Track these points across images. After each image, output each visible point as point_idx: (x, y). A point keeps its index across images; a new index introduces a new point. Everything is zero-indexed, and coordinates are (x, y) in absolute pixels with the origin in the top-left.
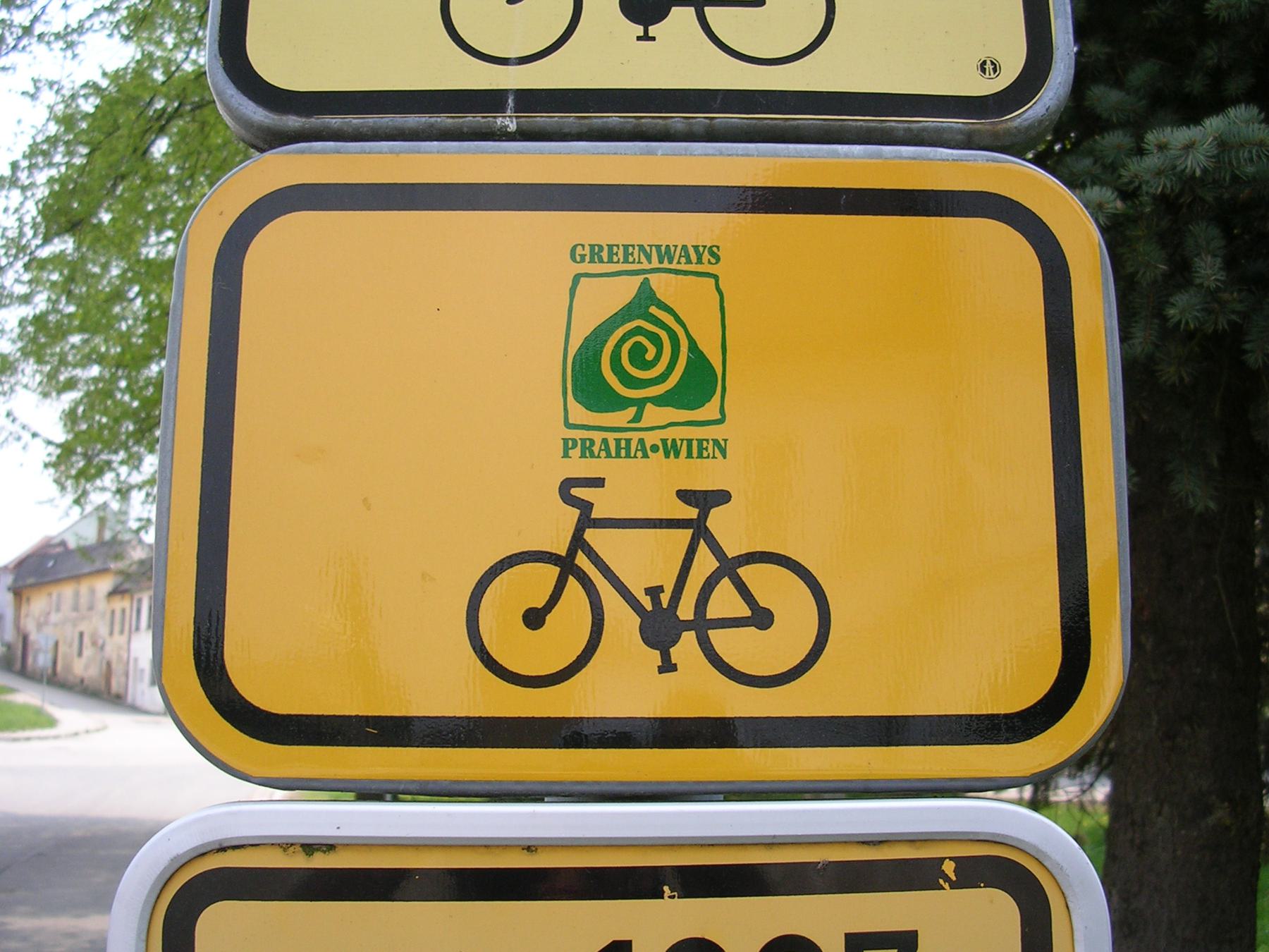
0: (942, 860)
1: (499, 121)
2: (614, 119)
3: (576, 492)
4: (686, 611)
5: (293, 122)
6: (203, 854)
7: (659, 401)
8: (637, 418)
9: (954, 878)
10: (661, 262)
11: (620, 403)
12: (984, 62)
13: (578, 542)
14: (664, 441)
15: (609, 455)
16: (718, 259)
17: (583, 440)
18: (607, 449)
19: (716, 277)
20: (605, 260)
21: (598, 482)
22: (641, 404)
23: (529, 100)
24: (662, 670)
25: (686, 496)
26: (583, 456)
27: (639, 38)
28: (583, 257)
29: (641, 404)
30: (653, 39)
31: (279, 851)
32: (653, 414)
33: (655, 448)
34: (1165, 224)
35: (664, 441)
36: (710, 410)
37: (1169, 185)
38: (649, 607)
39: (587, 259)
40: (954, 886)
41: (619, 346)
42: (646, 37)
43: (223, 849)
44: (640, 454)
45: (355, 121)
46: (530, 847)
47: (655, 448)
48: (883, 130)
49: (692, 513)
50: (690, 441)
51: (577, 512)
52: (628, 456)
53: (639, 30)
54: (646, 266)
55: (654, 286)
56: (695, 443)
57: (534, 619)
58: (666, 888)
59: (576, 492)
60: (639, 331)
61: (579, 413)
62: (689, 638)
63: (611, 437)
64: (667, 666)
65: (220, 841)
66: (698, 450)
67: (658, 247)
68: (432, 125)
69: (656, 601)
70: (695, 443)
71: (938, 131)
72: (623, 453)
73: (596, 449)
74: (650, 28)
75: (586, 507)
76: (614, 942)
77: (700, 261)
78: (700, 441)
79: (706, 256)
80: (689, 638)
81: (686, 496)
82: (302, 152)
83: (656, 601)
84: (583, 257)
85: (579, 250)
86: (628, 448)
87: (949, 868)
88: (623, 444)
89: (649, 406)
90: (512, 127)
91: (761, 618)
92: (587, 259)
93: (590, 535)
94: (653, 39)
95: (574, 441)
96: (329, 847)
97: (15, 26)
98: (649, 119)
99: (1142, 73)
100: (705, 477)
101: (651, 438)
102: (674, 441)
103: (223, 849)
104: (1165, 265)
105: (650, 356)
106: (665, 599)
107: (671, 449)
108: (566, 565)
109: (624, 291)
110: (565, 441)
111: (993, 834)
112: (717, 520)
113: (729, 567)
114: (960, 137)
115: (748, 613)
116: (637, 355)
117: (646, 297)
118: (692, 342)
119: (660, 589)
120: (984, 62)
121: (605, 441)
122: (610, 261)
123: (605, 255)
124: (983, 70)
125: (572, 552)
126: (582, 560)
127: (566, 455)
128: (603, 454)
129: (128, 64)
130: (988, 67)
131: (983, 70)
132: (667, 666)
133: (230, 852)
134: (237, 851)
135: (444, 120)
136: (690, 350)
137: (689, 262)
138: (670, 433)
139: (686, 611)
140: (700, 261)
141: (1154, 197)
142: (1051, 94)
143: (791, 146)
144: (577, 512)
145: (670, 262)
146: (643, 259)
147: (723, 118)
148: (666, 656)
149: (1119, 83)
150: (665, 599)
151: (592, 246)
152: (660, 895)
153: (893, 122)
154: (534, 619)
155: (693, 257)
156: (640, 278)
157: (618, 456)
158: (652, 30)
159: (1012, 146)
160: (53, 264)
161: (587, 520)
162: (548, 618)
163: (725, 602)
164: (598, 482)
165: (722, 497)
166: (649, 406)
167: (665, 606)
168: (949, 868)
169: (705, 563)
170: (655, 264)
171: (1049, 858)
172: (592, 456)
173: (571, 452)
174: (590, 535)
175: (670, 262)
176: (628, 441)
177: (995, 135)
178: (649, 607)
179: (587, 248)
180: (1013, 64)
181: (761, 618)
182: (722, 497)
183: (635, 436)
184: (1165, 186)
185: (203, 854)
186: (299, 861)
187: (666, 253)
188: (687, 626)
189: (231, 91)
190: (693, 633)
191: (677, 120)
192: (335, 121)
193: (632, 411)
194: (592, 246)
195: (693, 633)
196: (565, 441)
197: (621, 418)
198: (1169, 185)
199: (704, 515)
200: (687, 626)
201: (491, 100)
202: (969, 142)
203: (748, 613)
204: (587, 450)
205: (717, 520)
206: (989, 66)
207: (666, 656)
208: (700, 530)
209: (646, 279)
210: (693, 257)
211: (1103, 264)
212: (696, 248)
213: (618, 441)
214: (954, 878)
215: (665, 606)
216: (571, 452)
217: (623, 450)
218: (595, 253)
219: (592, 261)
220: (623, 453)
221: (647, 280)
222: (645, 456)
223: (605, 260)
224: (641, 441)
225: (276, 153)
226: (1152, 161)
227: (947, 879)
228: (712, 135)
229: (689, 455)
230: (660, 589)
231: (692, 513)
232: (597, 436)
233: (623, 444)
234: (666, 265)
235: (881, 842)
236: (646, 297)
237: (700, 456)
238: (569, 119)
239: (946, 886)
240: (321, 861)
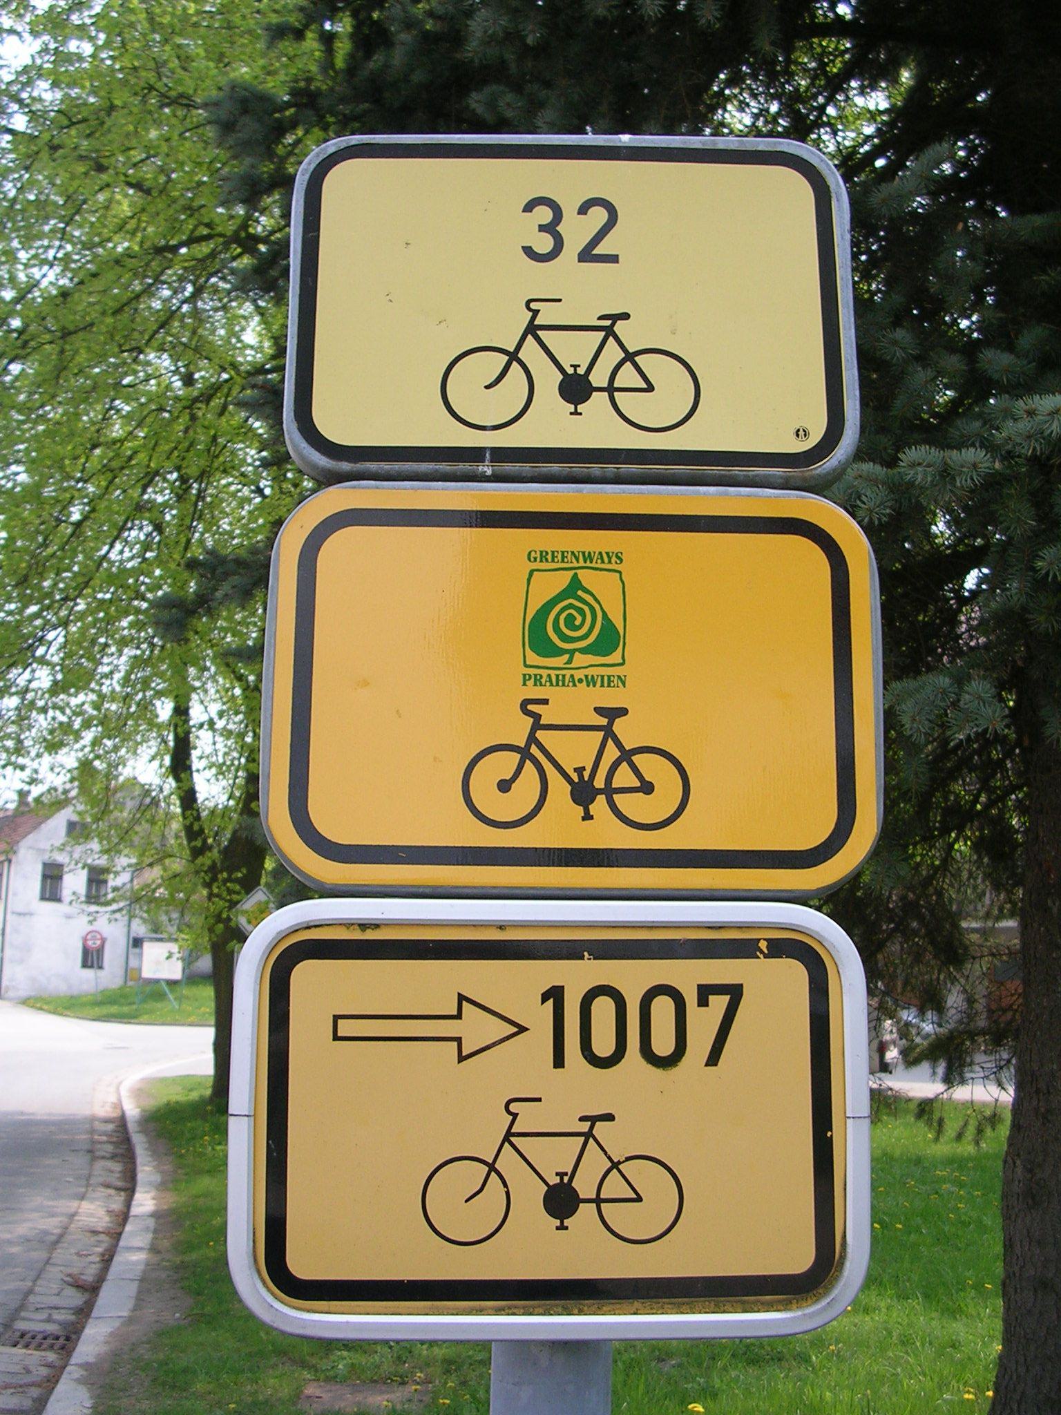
0: (759, 940)
1: (480, 468)
2: (555, 468)
3: (530, 707)
4: (599, 783)
5: (345, 466)
6: (297, 931)
7: (583, 651)
8: (570, 661)
9: (766, 951)
10: (585, 562)
11: (559, 652)
12: (799, 430)
13: (532, 739)
14: (586, 676)
15: (552, 685)
16: (621, 561)
17: (536, 675)
18: (551, 681)
19: (620, 572)
20: (550, 560)
21: (545, 702)
22: (572, 652)
23: (500, 454)
24: (584, 819)
25: (599, 711)
26: (535, 685)
27: (571, 414)
28: (535, 559)
29: (572, 652)
30: (581, 414)
31: (344, 928)
32: (579, 659)
33: (580, 681)
34: (1037, 483)
35: (586, 676)
36: (615, 657)
37: (1038, 448)
38: (576, 780)
39: (538, 560)
40: (766, 957)
41: (558, 615)
42: (576, 413)
43: (309, 928)
44: (571, 684)
45: (386, 466)
46: (501, 927)
47: (580, 681)
48: (731, 477)
49: (604, 721)
50: (603, 677)
51: (532, 720)
52: (563, 685)
53: (572, 408)
54: (576, 565)
55: (580, 578)
56: (606, 678)
57: (504, 786)
58: (586, 954)
59: (530, 707)
60: (571, 606)
61: (533, 658)
62: (601, 799)
63: (553, 673)
64: (588, 817)
65: (308, 922)
66: (608, 682)
67: (584, 553)
68: (437, 470)
69: (581, 776)
70: (606, 678)
71: (766, 476)
72: (560, 683)
73: (543, 681)
74: (579, 406)
75: (537, 717)
76: (554, 987)
77: (610, 562)
78: (609, 677)
79: (614, 559)
80: (601, 799)
81: (599, 711)
82: (354, 487)
83: (581, 776)
84: (535, 559)
85: (533, 554)
86: (564, 681)
87: (763, 945)
88: (560, 678)
89: (577, 653)
90: (489, 472)
91: (647, 788)
92: (538, 560)
93: (540, 734)
94: (581, 414)
95: (530, 675)
96: (376, 926)
97: (983, 1032)
98: (578, 468)
99: (1031, 337)
100: (611, 699)
101: (578, 675)
102: (593, 676)
103: (309, 928)
104: (1035, 521)
105: (577, 623)
106: (586, 775)
107: (591, 681)
108: (525, 753)
109: (564, 579)
110: (524, 675)
111: (791, 924)
112: (619, 726)
113: (626, 756)
114: (780, 481)
115: (639, 784)
116: (570, 621)
117: (575, 584)
118: (604, 614)
119: (584, 768)
120: (799, 430)
121: (549, 676)
122: (553, 561)
123: (549, 558)
124: (798, 435)
125: (528, 745)
126: (534, 750)
127: (524, 684)
128: (548, 684)
129: (314, 491)
130: (801, 433)
131: (798, 435)
132: (588, 817)
133: (313, 929)
134: (318, 929)
135: (444, 467)
136: (603, 619)
137: (603, 562)
138: (590, 672)
139: (599, 783)
140: (610, 562)
141: (1028, 459)
142: (842, 452)
143: (670, 487)
144: (532, 720)
145: (591, 562)
146: (574, 560)
147: (625, 468)
148: (587, 811)
149: (1010, 348)
150: (586, 775)
151: (541, 552)
152: (582, 958)
153: (736, 470)
154: (504, 786)
155: (606, 559)
156: (572, 572)
157: (557, 685)
158: (580, 408)
159: (819, 487)
160: (1024, 886)
161: (537, 725)
162: (513, 785)
163: (624, 777)
164: (545, 702)
165: (623, 712)
166: (577, 653)
167: (586, 779)
168: (763, 945)
169: (612, 753)
170: (582, 563)
171: (827, 940)
172: (541, 685)
173: (528, 683)
174: (540, 734)
175: (591, 562)
176: (564, 676)
177: (805, 479)
178: (576, 780)
179: (538, 553)
180: (818, 431)
181: (647, 788)
182: (623, 712)
183: (568, 673)
184: (1034, 449)
185: (297, 931)
186: (357, 935)
187: (588, 557)
188: (600, 792)
189: (303, 444)
190: (604, 796)
191: (595, 469)
192: (373, 466)
193: (567, 656)
194: (541, 552)
195: (604, 796)
196: (524, 675)
197: (560, 661)
198: (1038, 448)
199: (611, 723)
200: (600, 792)
201: (475, 454)
202: (786, 485)
203: (639, 784)
204: (538, 681)
205: (619, 726)
206: (801, 433)
207: (587, 811)
208: (609, 732)
209: (576, 574)
210: (606, 559)
211: (871, 565)
212: (607, 553)
213: (557, 676)
214: (766, 951)
215: (586, 779)
216: (528, 683)
217: (560, 682)
218: (543, 556)
219: (541, 561)
220: (560, 683)
221: (576, 574)
222: (575, 685)
223: (550, 560)
224: (572, 676)
225: (342, 487)
226: (1024, 425)
227: (762, 952)
228: (618, 480)
229: (602, 686)
230: (584, 768)
231: (604, 721)
232: (545, 673)
233: (560, 678)
234: (588, 564)
235: (720, 927)
236: (575, 584)
237: (609, 686)
238: (526, 468)
239: (761, 956)
240: (370, 935)
